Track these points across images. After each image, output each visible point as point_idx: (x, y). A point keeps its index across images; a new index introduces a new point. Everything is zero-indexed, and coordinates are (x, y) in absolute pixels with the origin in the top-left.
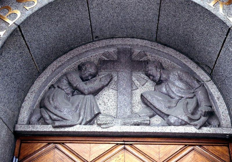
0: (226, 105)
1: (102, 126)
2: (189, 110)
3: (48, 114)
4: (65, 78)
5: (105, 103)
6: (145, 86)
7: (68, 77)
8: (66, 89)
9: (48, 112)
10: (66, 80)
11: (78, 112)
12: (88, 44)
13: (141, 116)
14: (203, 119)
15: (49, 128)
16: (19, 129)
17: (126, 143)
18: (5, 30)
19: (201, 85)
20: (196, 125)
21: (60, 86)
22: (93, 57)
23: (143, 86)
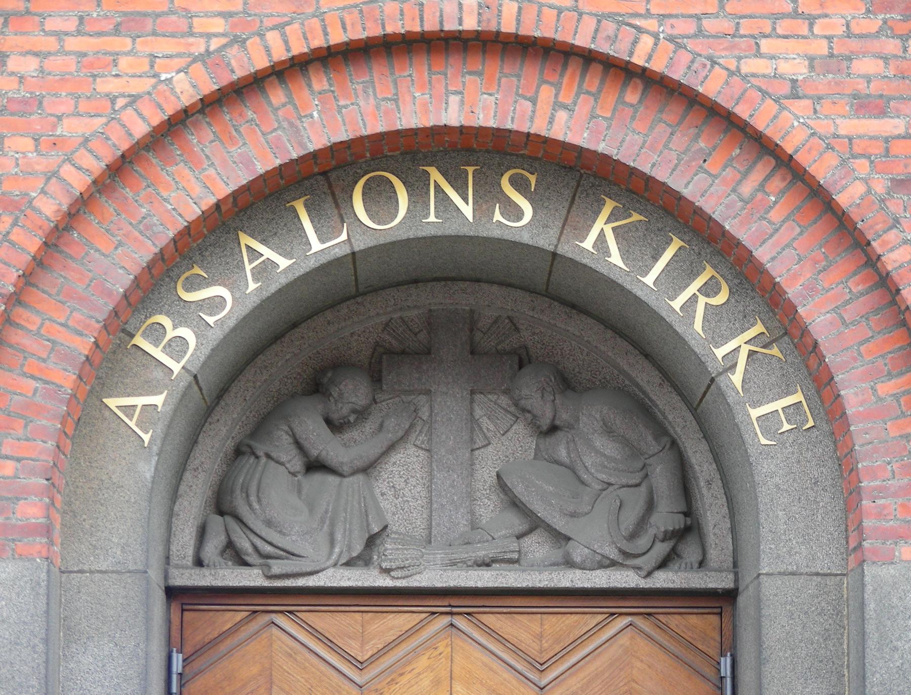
0: (726, 504)
1: (392, 574)
2: (623, 527)
3: (251, 541)
4: (286, 428)
5: (395, 491)
6: (510, 434)
7: (293, 426)
8: (289, 461)
9: (248, 532)
10: (287, 433)
11: (326, 528)
12: (344, 305)
13: (496, 537)
14: (661, 549)
15: (252, 578)
16: (178, 580)
17: (455, 610)
18: (166, 392)
19: (664, 448)
20: (639, 568)
21: (274, 455)
22: (356, 337)
23: (503, 435)
